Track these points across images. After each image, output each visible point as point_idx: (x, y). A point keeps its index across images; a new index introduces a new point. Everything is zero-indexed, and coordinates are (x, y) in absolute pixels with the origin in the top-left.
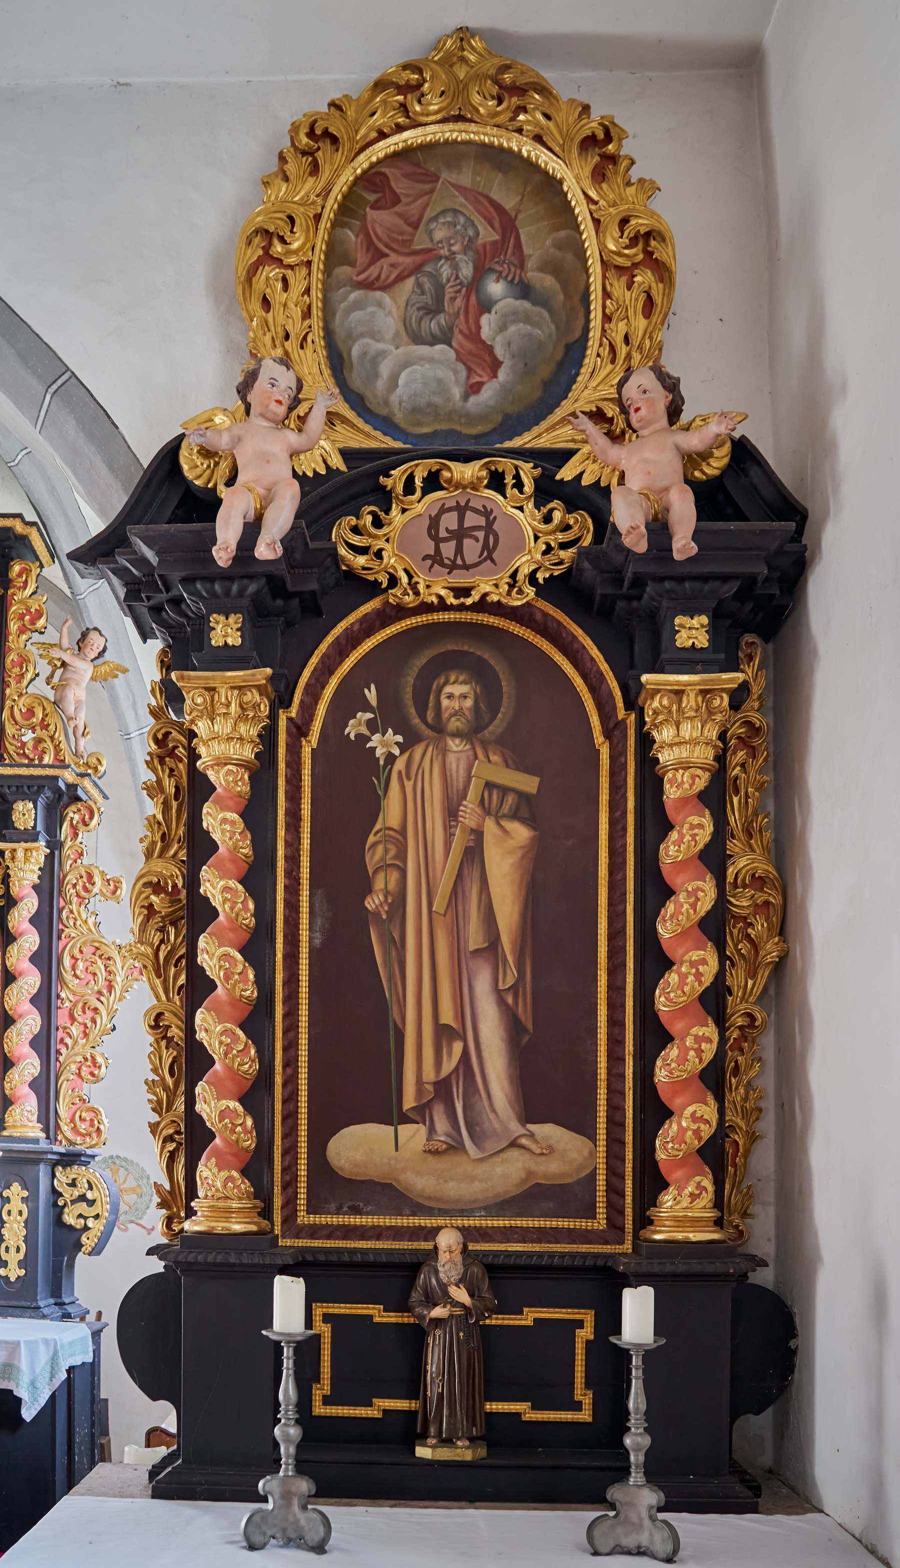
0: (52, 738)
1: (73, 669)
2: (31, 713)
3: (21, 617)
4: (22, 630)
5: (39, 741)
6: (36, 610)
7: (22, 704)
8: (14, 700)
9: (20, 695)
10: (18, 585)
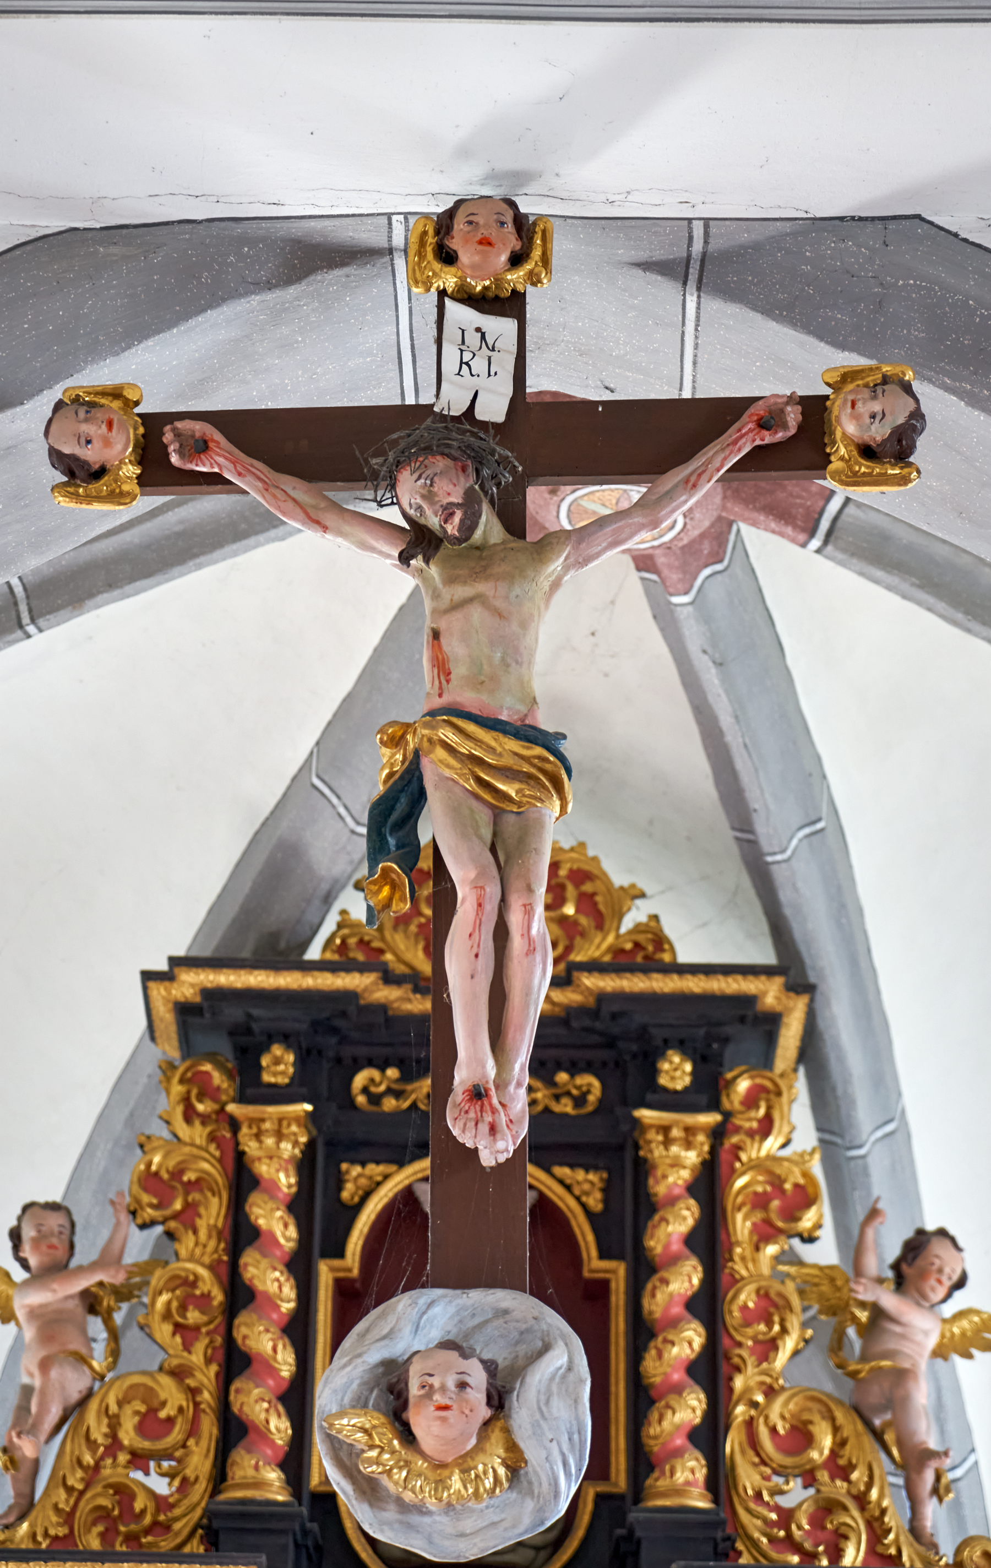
0: (861, 1500)
1: (897, 1329)
2: (801, 1436)
3: (760, 1202)
4: (765, 1233)
5: (827, 1508)
6: (797, 1186)
7: (779, 1413)
8: (755, 1405)
9: (771, 1392)
10: (747, 1125)
